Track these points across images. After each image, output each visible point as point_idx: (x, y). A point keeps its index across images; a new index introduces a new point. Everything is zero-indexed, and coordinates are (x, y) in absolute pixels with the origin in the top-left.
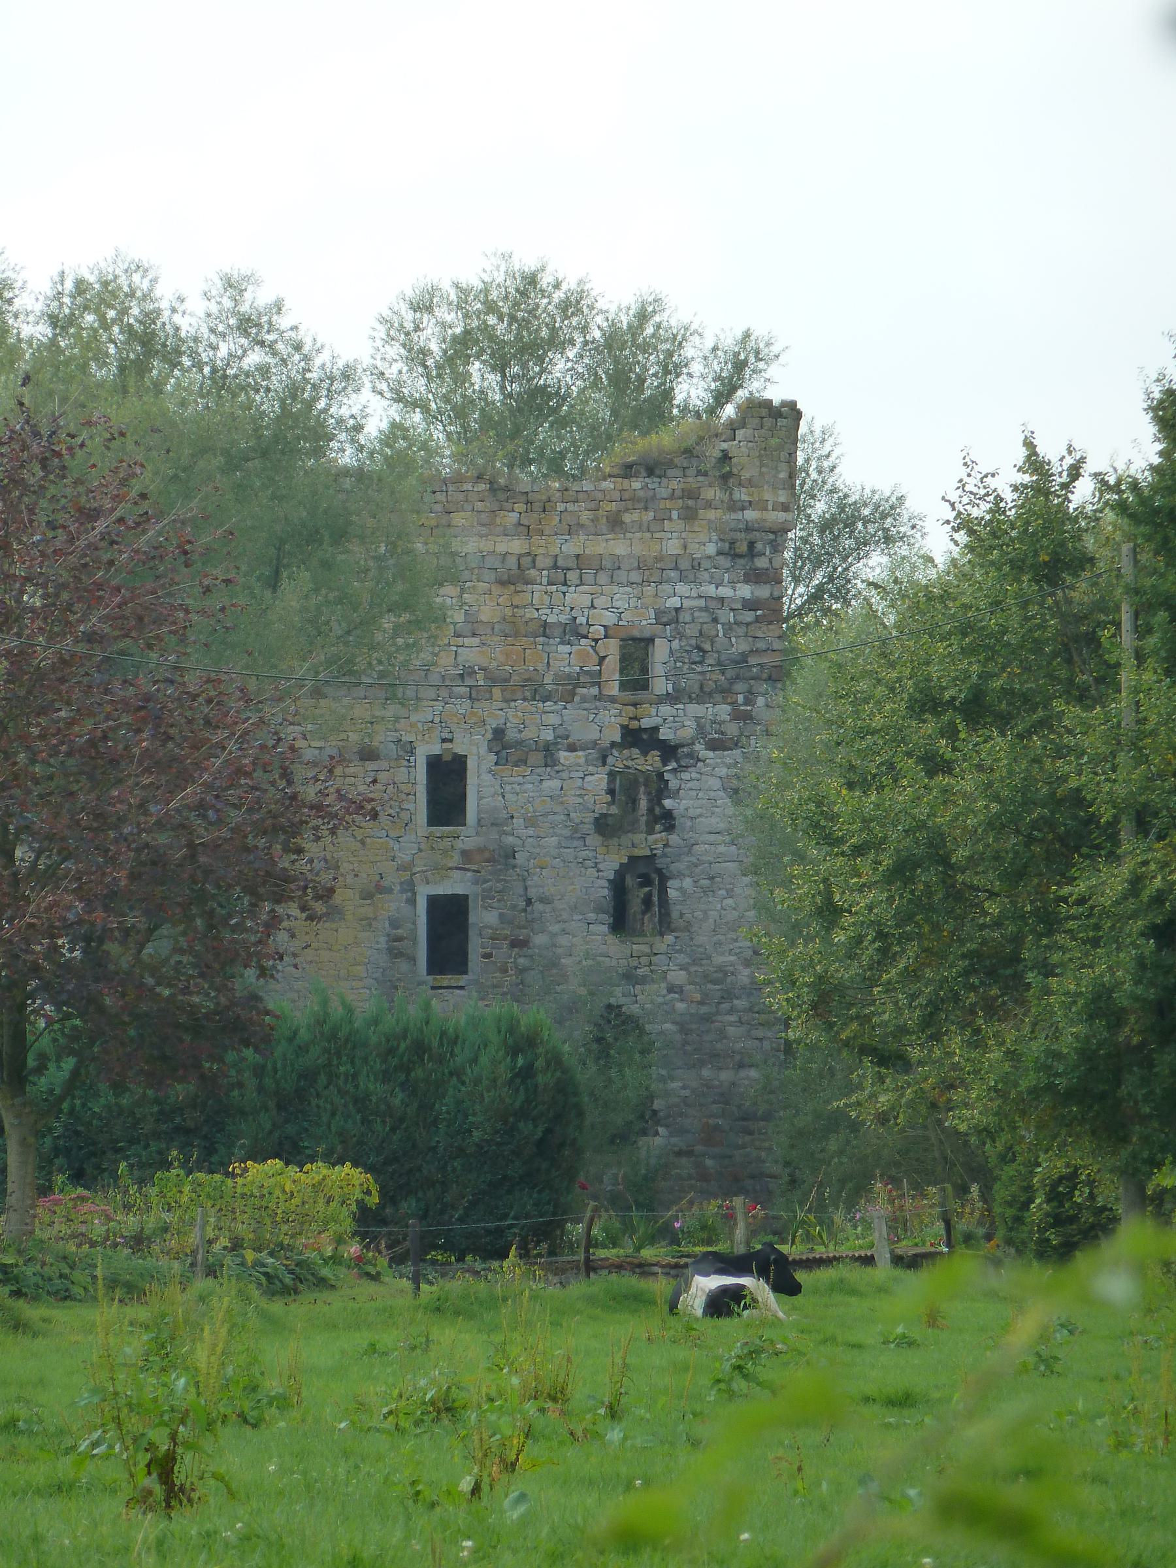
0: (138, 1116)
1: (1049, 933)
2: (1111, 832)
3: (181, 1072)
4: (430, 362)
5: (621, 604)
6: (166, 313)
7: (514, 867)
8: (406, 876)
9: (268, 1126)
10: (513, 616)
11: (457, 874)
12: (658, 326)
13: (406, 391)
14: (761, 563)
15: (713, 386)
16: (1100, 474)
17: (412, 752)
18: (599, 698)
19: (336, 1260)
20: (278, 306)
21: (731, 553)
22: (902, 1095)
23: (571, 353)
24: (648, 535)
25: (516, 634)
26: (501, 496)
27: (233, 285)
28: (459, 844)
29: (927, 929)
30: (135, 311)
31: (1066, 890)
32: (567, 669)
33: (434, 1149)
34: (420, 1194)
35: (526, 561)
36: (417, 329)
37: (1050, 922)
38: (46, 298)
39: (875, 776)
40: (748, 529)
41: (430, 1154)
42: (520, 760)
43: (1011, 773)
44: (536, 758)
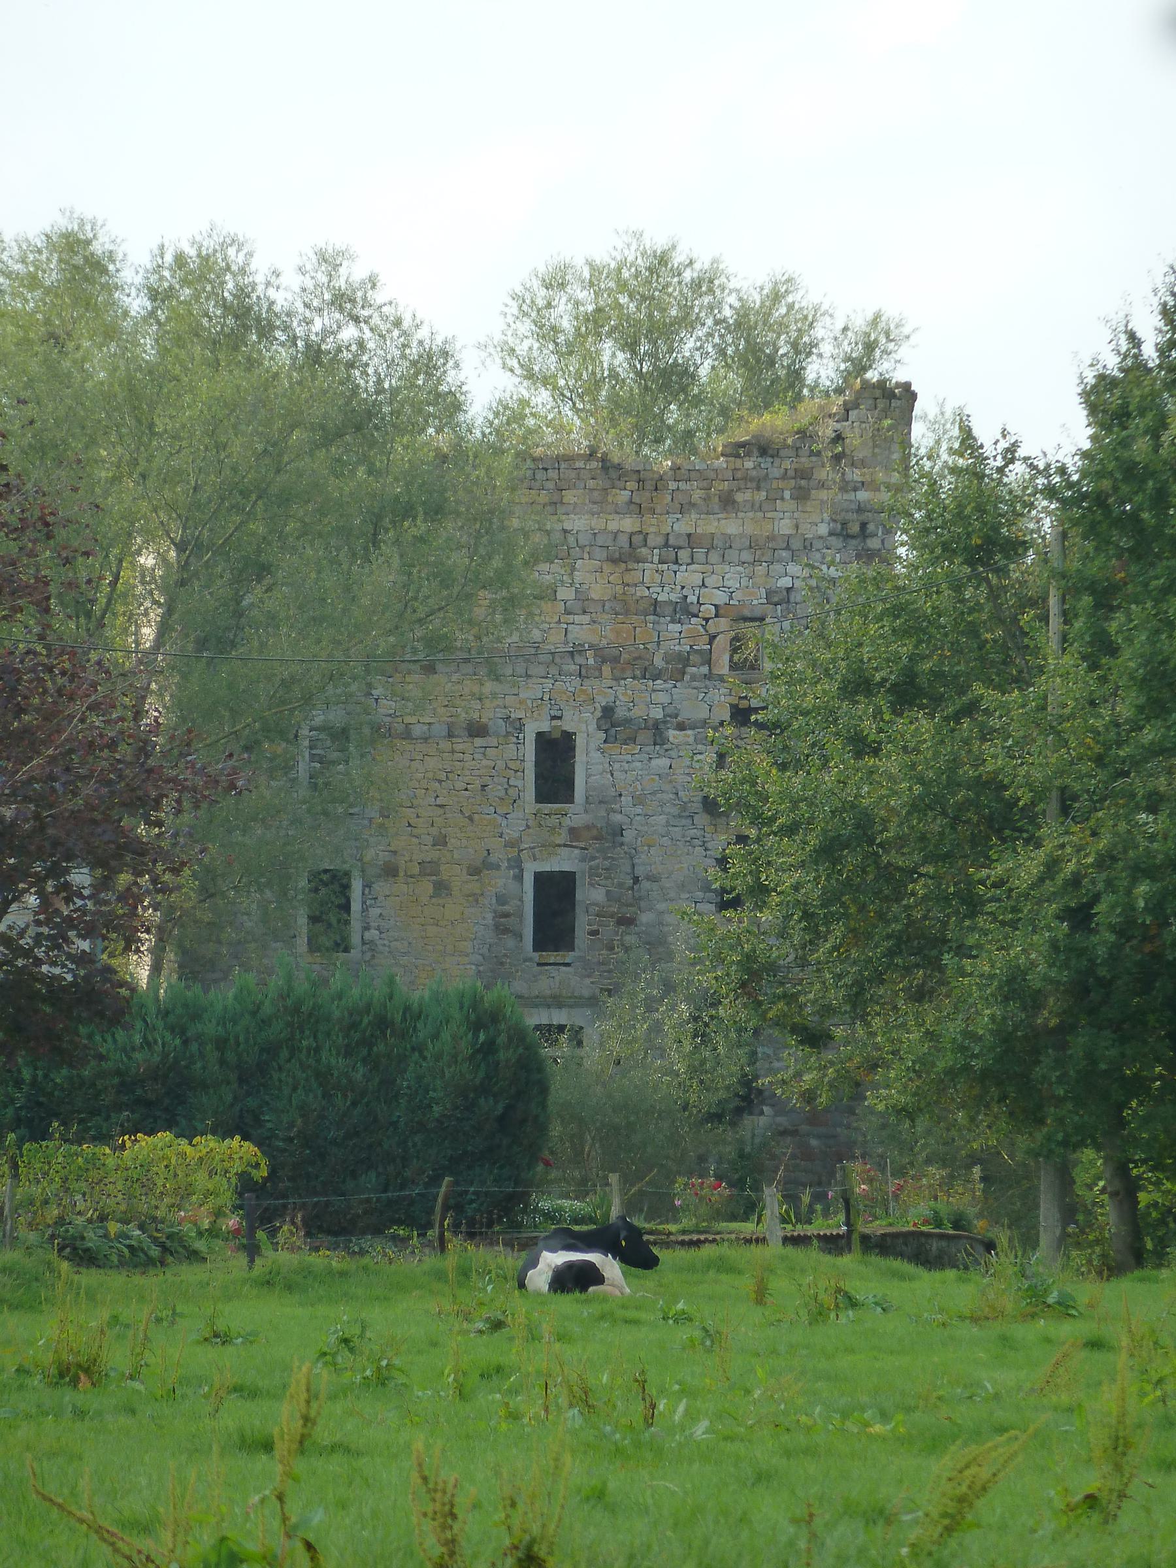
0: (100, 1087)
1: (972, 915)
2: (1030, 814)
3: (32, 1044)
4: (561, 339)
5: (732, 583)
6: (260, 289)
7: (622, 844)
8: (513, 853)
9: (229, 1098)
10: (624, 594)
11: (564, 851)
12: (790, 307)
13: (536, 368)
14: (874, 543)
15: (843, 366)
16: (1029, 458)
17: (521, 729)
18: (708, 677)
19: (213, 1233)
20: (373, 282)
21: (842, 533)
22: (825, 1075)
23: (701, 332)
24: (760, 514)
25: (627, 613)
26: (613, 474)
27: (329, 261)
28: (566, 822)
29: (853, 910)
30: (230, 285)
31: (984, 872)
32: (677, 648)
33: (394, 1124)
34: (380, 1170)
35: (637, 539)
36: (549, 306)
37: (972, 905)
38: (147, 271)
39: (808, 756)
40: (860, 510)
41: (391, 1129)
42: (630, 739)
43: (936, 755)
44: (644, 736)
